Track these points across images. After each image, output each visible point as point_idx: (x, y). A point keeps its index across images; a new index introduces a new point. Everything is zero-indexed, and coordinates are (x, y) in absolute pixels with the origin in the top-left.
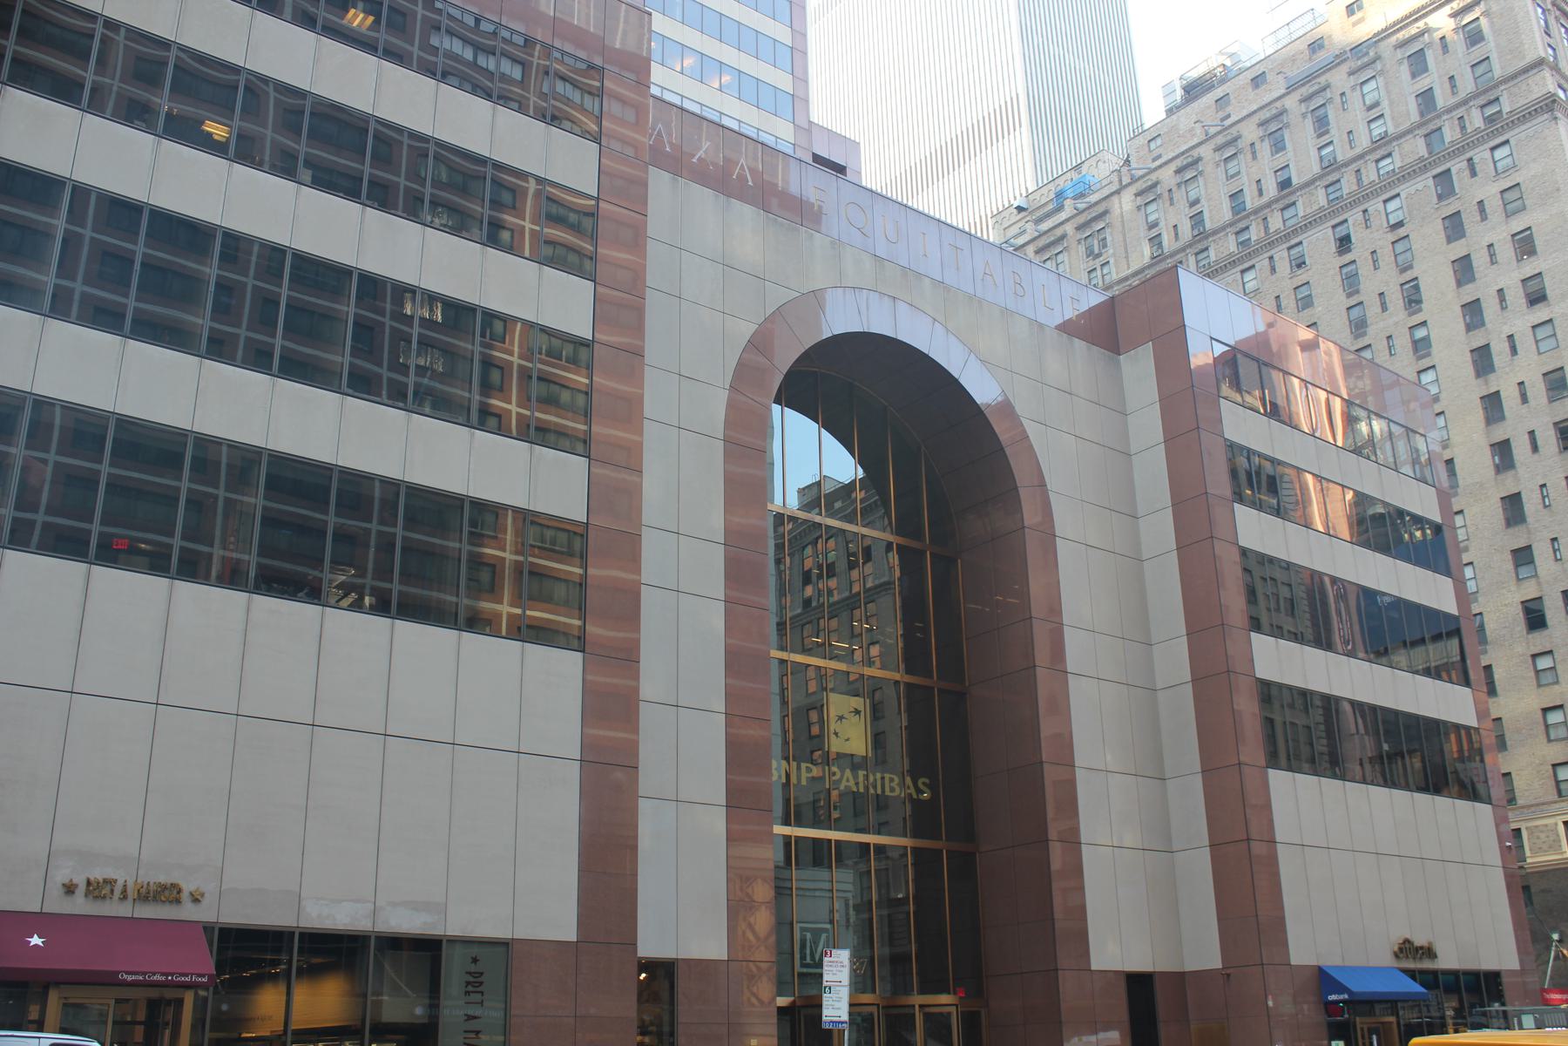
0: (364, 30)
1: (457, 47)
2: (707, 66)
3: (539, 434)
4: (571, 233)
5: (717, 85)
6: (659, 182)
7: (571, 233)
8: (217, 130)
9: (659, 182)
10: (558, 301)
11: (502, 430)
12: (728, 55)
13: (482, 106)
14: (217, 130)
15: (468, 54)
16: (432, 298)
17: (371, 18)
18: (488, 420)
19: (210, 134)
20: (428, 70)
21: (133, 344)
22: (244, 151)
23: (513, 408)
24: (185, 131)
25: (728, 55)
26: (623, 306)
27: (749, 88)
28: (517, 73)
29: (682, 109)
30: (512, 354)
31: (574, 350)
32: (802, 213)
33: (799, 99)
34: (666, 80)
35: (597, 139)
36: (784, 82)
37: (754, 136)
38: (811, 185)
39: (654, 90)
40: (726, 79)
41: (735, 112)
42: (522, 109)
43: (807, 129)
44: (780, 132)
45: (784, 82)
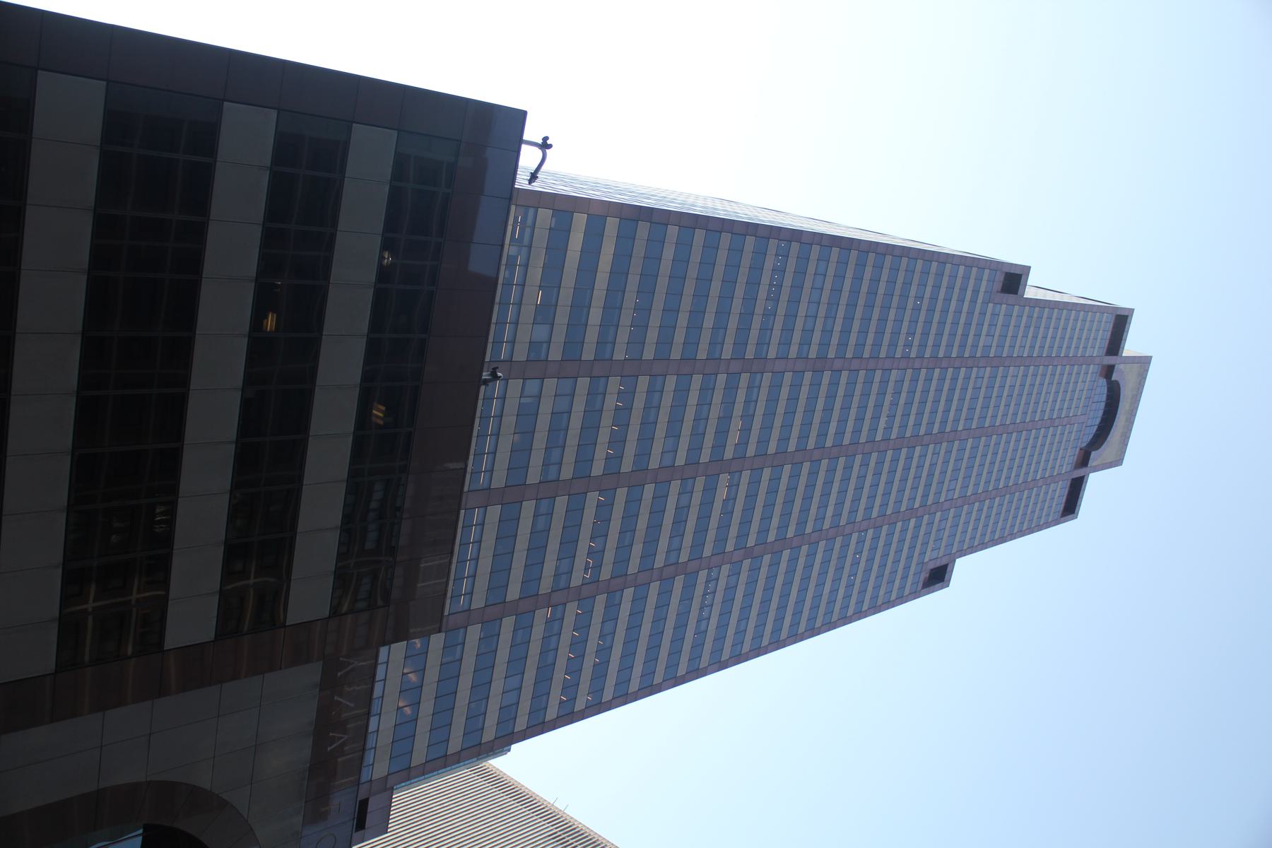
0: (374, 419)
1: (378, 495)
2: (413, 692)
3: (70, 629)
4: (253, 610)
5: (401, 704)
6: (311, 673)
7: (253, 610)
8: (270, 322)
9: (311, 673)
10: (191, 615)
11: (65, 599)
12: (427, 707)
13: (336, 518)
14: (270, 322)
15: (374, 505)
16: (171, 523)
17: (381, 422)
18: (74, 581)
19: (267, 317)
20: (354, 474)
21: (83, 279)
22: (259, 347)
23: (90, 605)
24: (264, 301)
25: (427, 707)
26: (200, 668)
27: (406, 726)
28: (369, 545)
29: (364, 750)
30: (139, 592)
31: (154, 622)
32: (316, 810)
33: (410, 774)
34: (393, 657)
35: (335, 612)
36: (418, 758)
37: (368, 746)
38: (342, 802)
39: (383, 656)
40: (408, 710)
41: (382, 726)
42: (341, 556)
43: (387, 788)
44: (377, 766)
45: (418, 758)
